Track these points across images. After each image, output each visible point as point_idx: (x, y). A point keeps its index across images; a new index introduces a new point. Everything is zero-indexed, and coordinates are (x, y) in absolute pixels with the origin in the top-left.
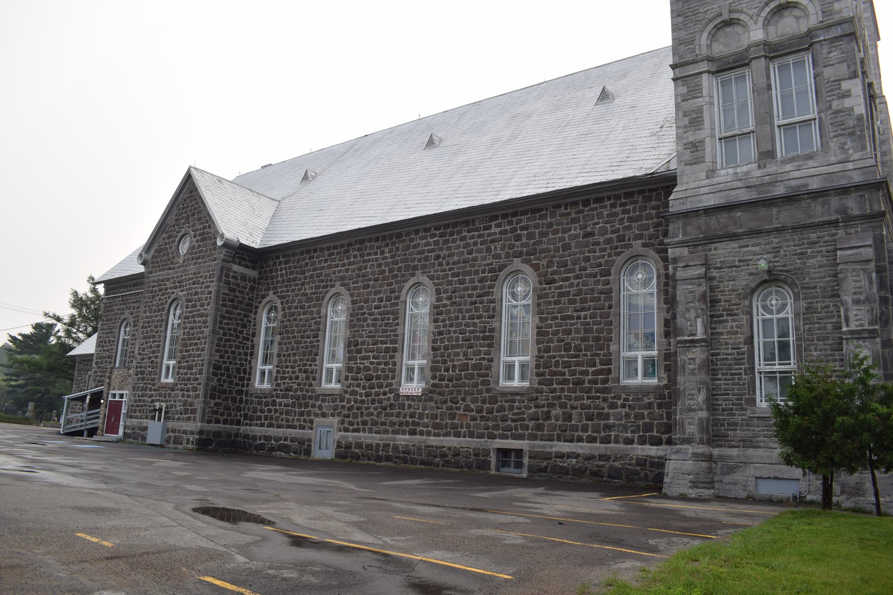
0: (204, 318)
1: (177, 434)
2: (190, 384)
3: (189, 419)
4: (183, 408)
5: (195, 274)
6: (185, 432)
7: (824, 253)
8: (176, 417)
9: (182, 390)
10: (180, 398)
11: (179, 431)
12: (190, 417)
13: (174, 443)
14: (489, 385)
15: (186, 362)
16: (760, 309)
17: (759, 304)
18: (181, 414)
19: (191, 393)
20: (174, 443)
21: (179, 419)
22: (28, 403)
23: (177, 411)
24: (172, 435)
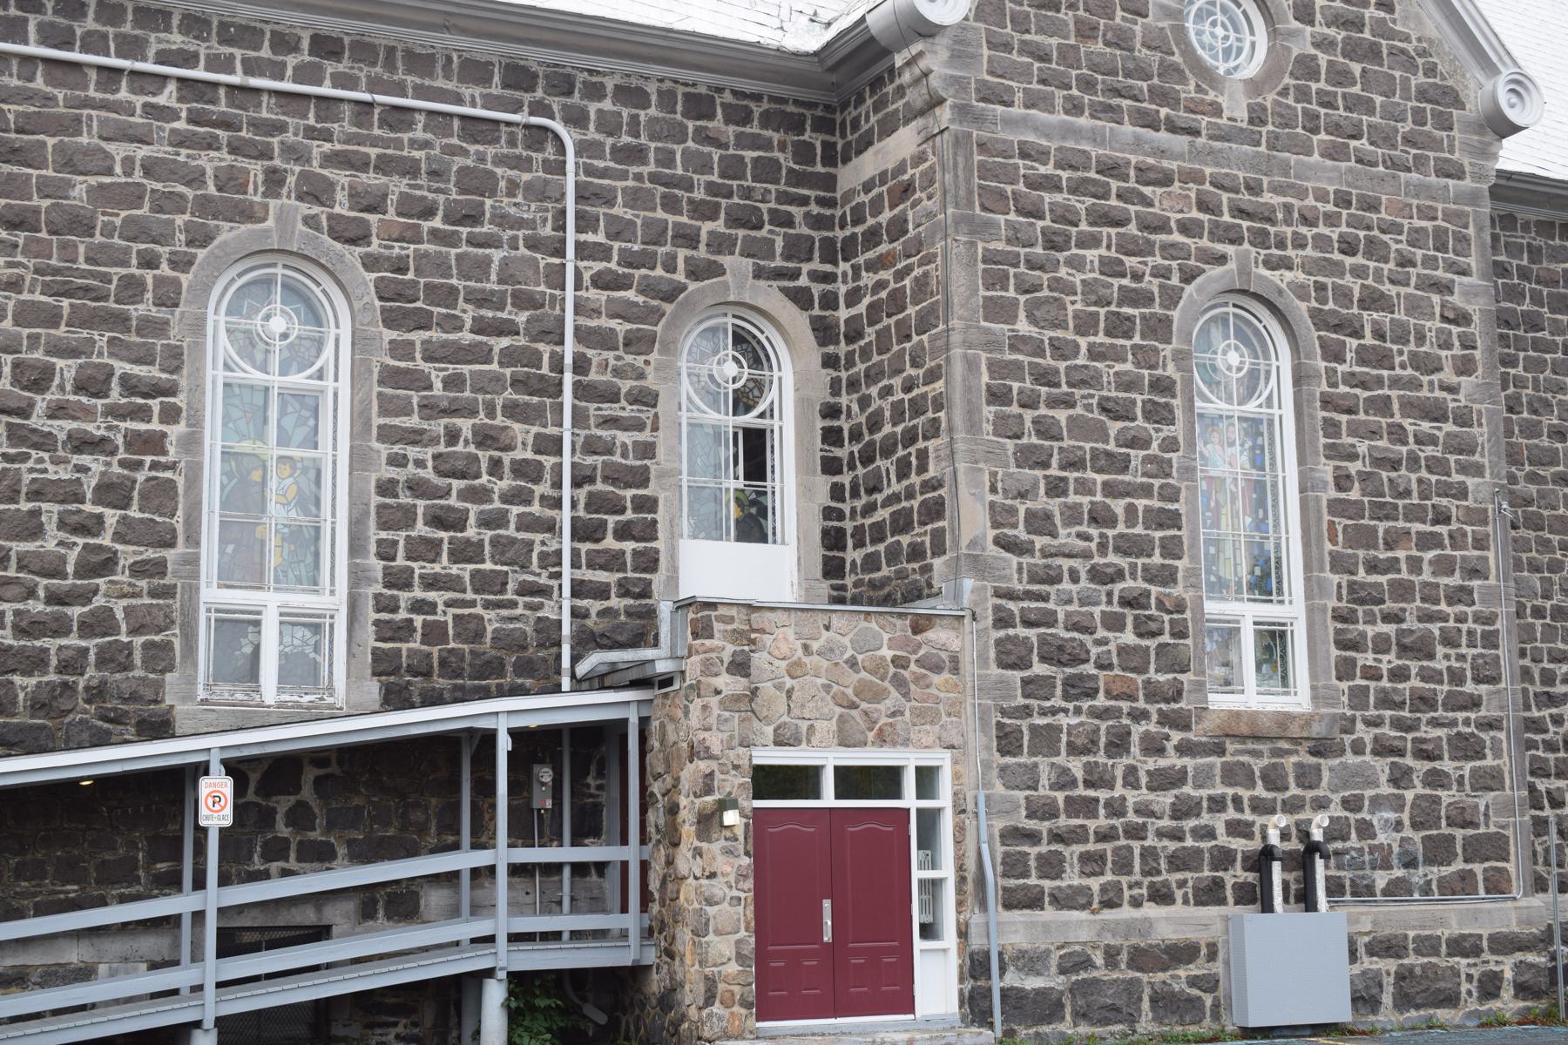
0: (1449, 427)
1: (1411, 960)
2: (1435, 723)
3: (1461, 886)
4: (1417, 837)
5: (1343, 200)
6: (1463, 946)
7: (1132, 229)
8: (1381, 879)
9: (1383, 749)
10: (1386, 789)
11: (1428, 945)
12: (1466, 879)
13: (1404, 1001)
14: (163, 574)
15: (1388, 618)
16: (223, 335)
17: (222, 318)
18: (1410, 864)
19: (1447, 765)
20: (1404, 1001)
21: (1397, 889)
22: (1259, 871)
23: (1386, 851)
24: (1389, 965)
